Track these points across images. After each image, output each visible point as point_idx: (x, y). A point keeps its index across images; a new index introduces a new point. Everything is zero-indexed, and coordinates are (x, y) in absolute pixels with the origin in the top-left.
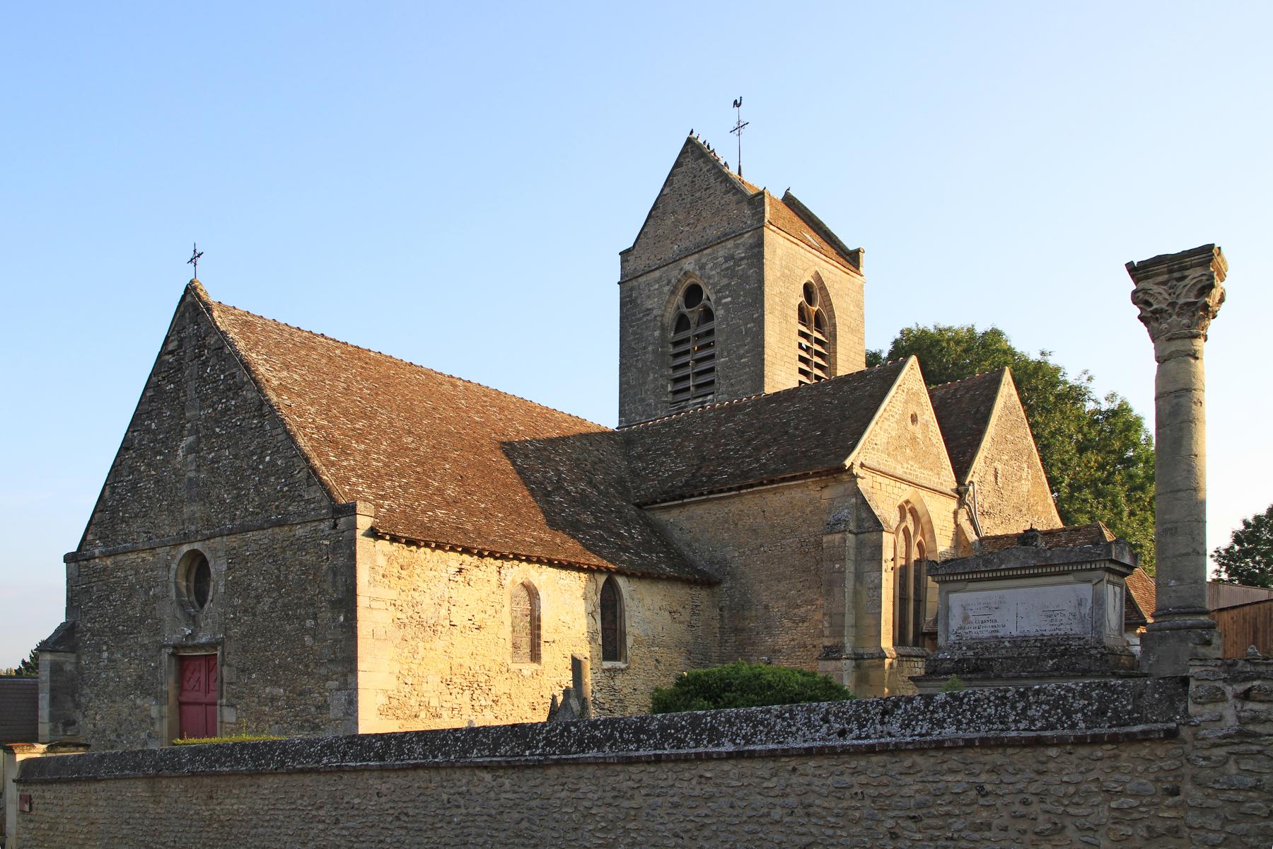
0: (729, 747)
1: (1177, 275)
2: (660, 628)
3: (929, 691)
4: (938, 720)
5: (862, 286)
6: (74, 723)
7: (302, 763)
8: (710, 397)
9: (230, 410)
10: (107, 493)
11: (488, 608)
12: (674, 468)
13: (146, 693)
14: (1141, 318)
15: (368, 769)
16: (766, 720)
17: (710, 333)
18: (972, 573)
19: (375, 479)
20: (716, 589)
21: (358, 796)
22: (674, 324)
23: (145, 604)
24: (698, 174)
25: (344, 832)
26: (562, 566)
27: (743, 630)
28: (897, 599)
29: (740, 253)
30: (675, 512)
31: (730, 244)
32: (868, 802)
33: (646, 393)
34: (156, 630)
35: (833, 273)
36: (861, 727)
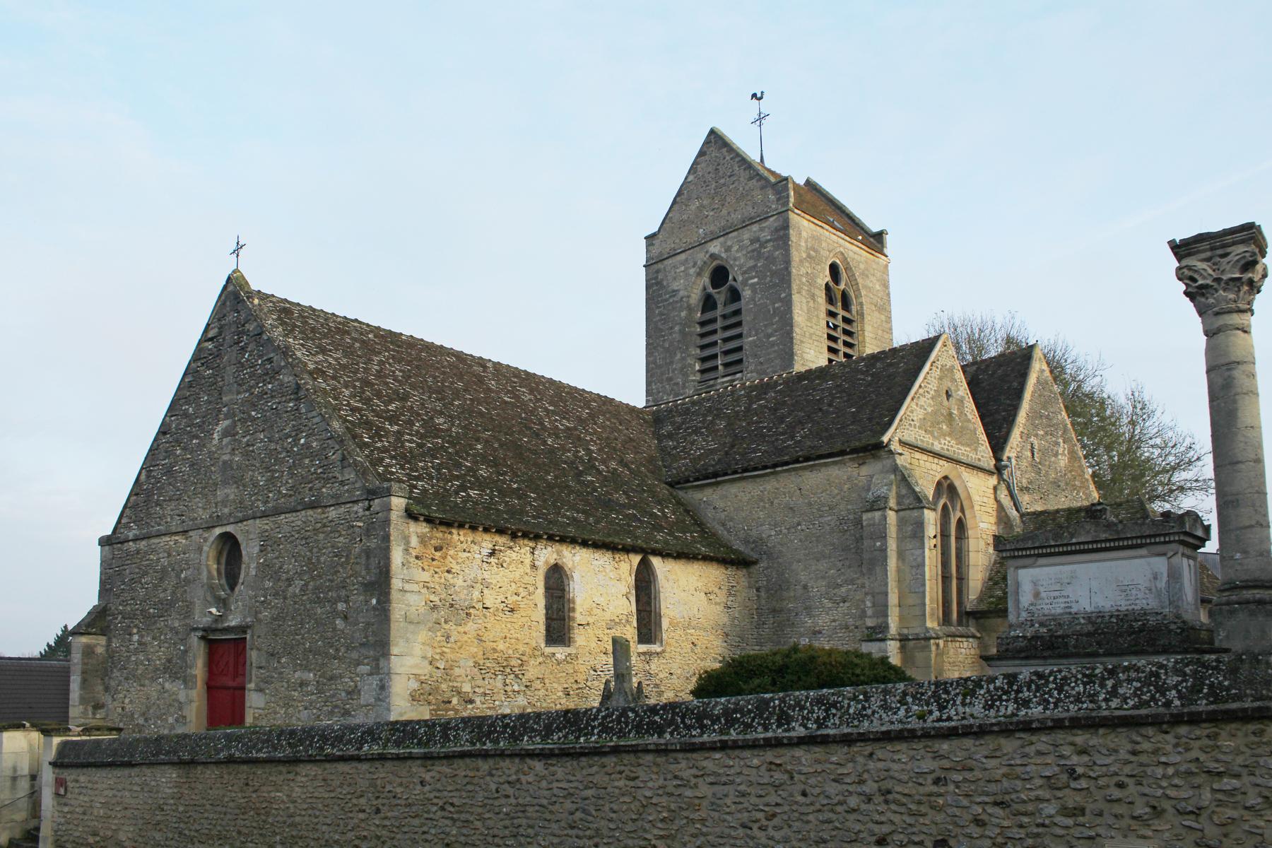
0: (800, 731)
1: (1220, 252)
2: (696, 610)
3: (1010, 670)
4: (1024, 700)
5: (886, 266)
6: (102, 706)
7: (342, 750)
8: (739, 375)
9: (266, 393)
10: (143, 477)
11: (521, 590)
12: (704, 446)
13: (174, 677)
14: (1186, 293)
15: (410, 757)
16: (840, 702)
17: (738, 312)
18: (1042, 547)
19: (406, 459)
20: (754, 569)
21: (401, 784)
22: (701, 304)
23: (176, 587)
24: (722, 162)
25: (387, 823)
26: (597, 546)
27: (781, 611)
28: (940, 578)
29: (766, 235)
30: (709, 491)
31: (755, 228)
32: (951, 787)
33: (673, 371)
34: (188, 612)
35: (855, 252)
36: (941, 708)
